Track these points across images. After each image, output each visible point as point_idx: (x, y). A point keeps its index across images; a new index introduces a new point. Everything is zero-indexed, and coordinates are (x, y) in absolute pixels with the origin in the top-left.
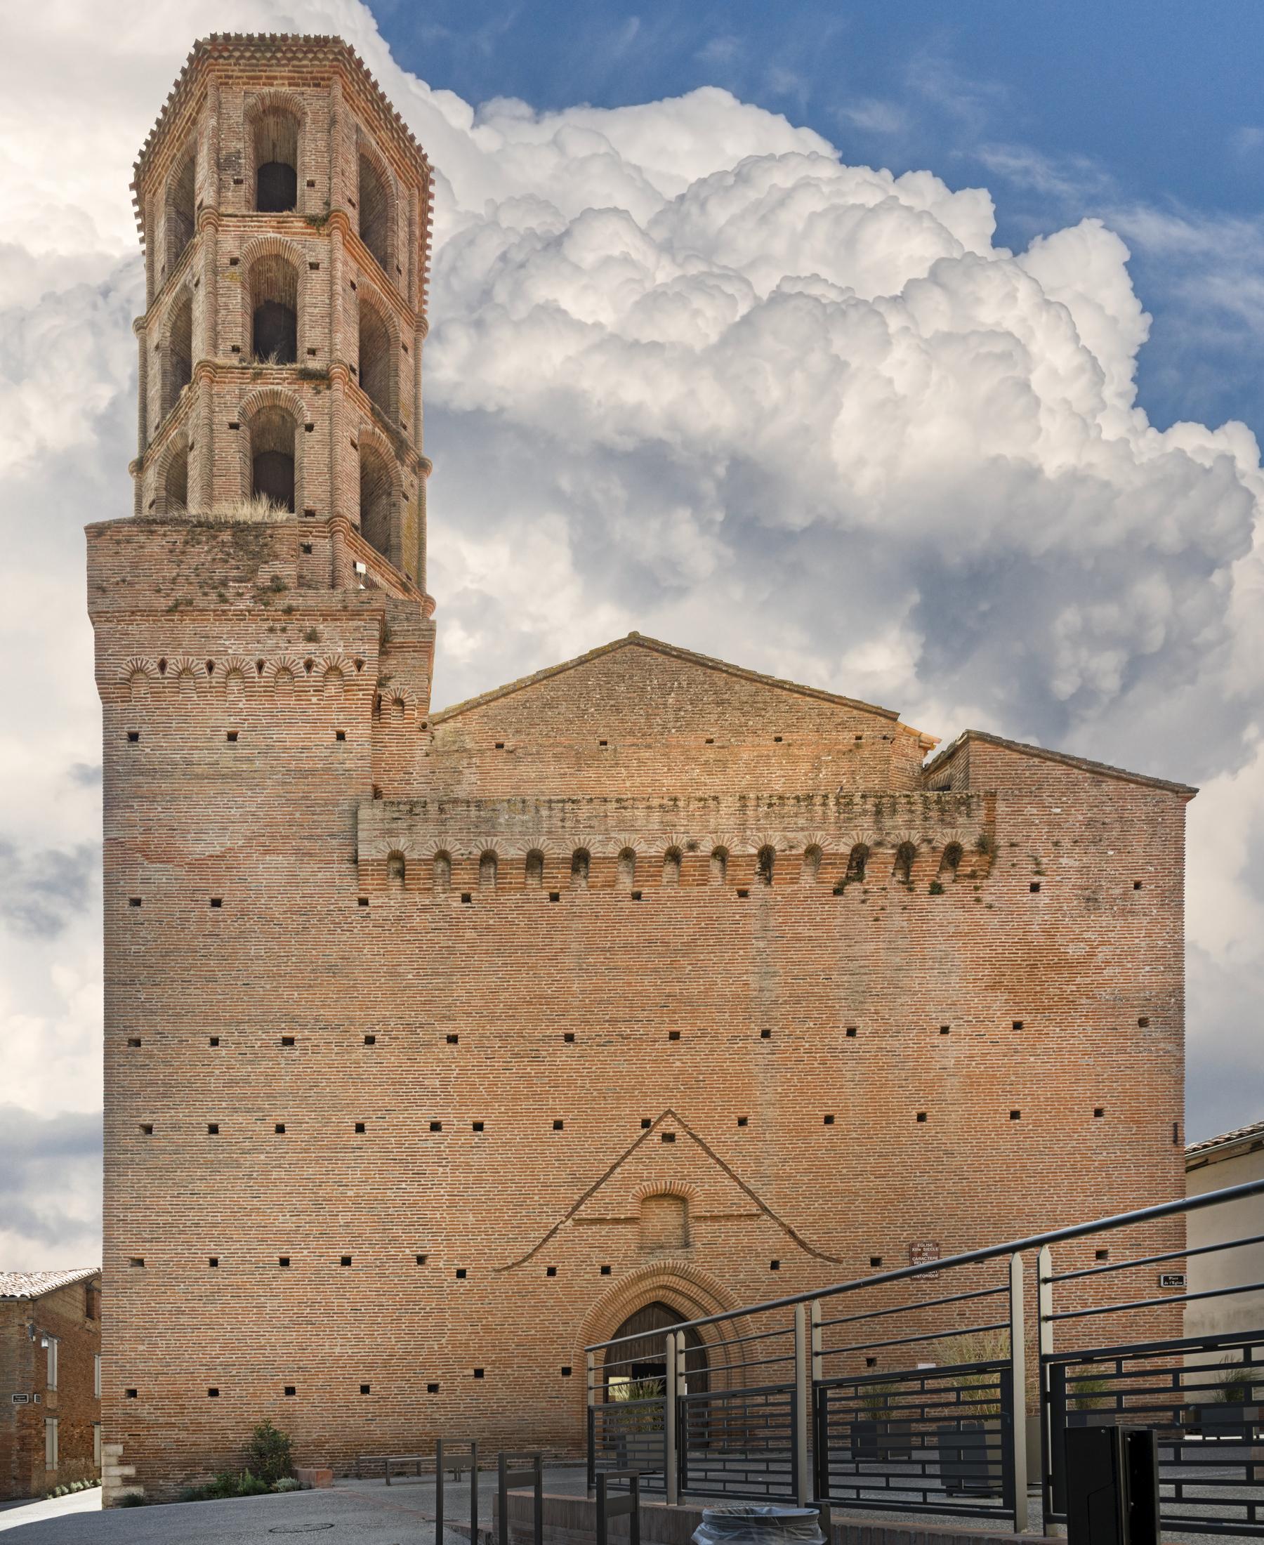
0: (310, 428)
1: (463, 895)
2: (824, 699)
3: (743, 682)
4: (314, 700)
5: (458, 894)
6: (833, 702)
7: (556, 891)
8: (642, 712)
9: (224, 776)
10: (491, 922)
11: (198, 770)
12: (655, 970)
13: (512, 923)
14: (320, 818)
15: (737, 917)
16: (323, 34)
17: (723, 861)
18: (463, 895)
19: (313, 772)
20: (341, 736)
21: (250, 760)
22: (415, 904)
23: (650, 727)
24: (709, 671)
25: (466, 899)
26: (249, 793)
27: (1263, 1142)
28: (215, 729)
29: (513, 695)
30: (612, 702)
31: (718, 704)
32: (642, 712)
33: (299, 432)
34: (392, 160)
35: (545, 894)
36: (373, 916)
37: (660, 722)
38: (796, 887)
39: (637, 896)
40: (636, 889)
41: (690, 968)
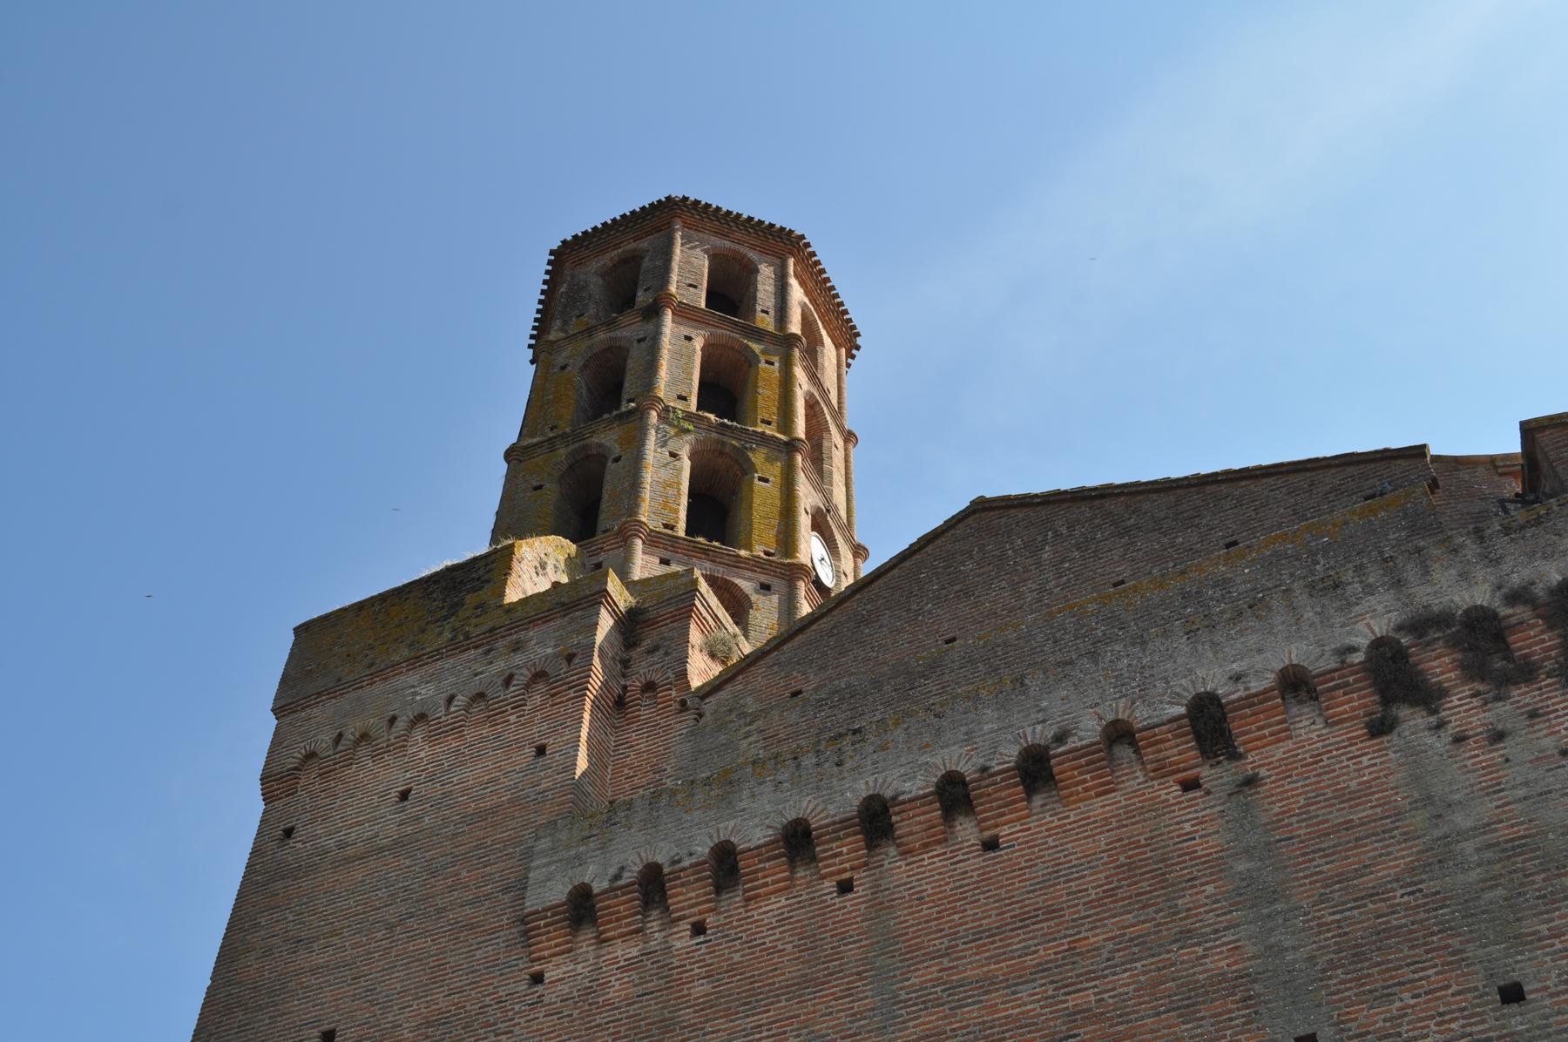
0: (617, 460)
1: (694, 925)
2: (1288, 472)
3: (1155, 496)
4: (513, 718)
5: (685, 926)
6: (1307, 470)
7: (846, 876)
8: (1004, 584)
9: (382, 849)
10: (737, 957)
11: (350, 851)
12: (1041, 969)
13: (774, 950)
14: (494, 869)
15: (1187, 827)
16: (655, 200)
17: (1133, 743)
18: (694, 925)
19: (493, 811)
20: (541, 751)
21: (418, 819)
22: (615, 961)
23: (1020, 596)
24: (1097, 503)
25: (699, 929)
26: (408, 862)
27: (1566, 950)
28: (387, 792)
29: (814, 627)
30: (957, 588)
31: (1121, 535)
32: (1004, 584)
33: (610, 465)
34: (617, 246)
35: (829, 885)
36: (546, 1000)
37: (1034, 586)
38: (1290, 744)
39: (991, 845)
40: (987, 834)
41: (1110, 945)
